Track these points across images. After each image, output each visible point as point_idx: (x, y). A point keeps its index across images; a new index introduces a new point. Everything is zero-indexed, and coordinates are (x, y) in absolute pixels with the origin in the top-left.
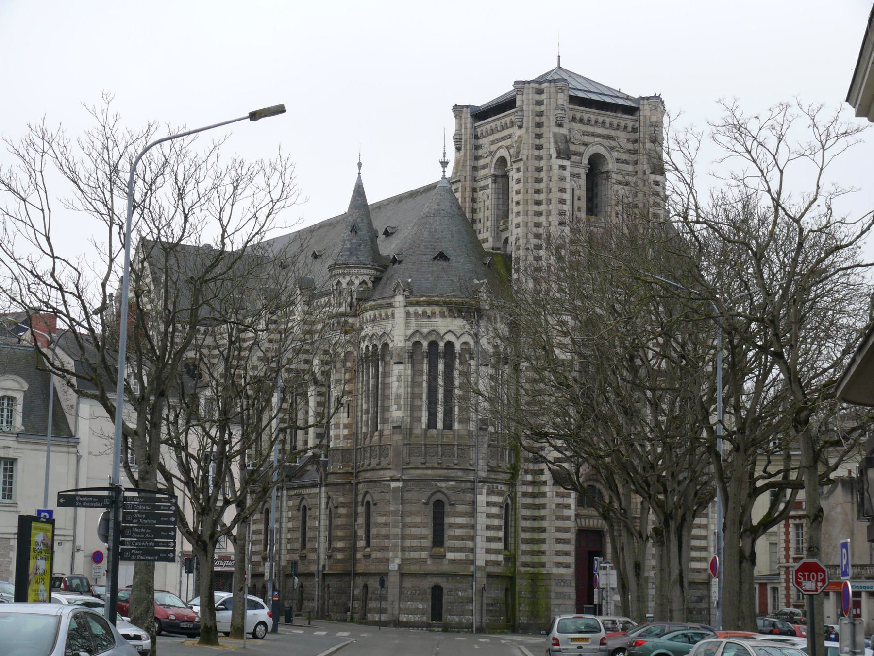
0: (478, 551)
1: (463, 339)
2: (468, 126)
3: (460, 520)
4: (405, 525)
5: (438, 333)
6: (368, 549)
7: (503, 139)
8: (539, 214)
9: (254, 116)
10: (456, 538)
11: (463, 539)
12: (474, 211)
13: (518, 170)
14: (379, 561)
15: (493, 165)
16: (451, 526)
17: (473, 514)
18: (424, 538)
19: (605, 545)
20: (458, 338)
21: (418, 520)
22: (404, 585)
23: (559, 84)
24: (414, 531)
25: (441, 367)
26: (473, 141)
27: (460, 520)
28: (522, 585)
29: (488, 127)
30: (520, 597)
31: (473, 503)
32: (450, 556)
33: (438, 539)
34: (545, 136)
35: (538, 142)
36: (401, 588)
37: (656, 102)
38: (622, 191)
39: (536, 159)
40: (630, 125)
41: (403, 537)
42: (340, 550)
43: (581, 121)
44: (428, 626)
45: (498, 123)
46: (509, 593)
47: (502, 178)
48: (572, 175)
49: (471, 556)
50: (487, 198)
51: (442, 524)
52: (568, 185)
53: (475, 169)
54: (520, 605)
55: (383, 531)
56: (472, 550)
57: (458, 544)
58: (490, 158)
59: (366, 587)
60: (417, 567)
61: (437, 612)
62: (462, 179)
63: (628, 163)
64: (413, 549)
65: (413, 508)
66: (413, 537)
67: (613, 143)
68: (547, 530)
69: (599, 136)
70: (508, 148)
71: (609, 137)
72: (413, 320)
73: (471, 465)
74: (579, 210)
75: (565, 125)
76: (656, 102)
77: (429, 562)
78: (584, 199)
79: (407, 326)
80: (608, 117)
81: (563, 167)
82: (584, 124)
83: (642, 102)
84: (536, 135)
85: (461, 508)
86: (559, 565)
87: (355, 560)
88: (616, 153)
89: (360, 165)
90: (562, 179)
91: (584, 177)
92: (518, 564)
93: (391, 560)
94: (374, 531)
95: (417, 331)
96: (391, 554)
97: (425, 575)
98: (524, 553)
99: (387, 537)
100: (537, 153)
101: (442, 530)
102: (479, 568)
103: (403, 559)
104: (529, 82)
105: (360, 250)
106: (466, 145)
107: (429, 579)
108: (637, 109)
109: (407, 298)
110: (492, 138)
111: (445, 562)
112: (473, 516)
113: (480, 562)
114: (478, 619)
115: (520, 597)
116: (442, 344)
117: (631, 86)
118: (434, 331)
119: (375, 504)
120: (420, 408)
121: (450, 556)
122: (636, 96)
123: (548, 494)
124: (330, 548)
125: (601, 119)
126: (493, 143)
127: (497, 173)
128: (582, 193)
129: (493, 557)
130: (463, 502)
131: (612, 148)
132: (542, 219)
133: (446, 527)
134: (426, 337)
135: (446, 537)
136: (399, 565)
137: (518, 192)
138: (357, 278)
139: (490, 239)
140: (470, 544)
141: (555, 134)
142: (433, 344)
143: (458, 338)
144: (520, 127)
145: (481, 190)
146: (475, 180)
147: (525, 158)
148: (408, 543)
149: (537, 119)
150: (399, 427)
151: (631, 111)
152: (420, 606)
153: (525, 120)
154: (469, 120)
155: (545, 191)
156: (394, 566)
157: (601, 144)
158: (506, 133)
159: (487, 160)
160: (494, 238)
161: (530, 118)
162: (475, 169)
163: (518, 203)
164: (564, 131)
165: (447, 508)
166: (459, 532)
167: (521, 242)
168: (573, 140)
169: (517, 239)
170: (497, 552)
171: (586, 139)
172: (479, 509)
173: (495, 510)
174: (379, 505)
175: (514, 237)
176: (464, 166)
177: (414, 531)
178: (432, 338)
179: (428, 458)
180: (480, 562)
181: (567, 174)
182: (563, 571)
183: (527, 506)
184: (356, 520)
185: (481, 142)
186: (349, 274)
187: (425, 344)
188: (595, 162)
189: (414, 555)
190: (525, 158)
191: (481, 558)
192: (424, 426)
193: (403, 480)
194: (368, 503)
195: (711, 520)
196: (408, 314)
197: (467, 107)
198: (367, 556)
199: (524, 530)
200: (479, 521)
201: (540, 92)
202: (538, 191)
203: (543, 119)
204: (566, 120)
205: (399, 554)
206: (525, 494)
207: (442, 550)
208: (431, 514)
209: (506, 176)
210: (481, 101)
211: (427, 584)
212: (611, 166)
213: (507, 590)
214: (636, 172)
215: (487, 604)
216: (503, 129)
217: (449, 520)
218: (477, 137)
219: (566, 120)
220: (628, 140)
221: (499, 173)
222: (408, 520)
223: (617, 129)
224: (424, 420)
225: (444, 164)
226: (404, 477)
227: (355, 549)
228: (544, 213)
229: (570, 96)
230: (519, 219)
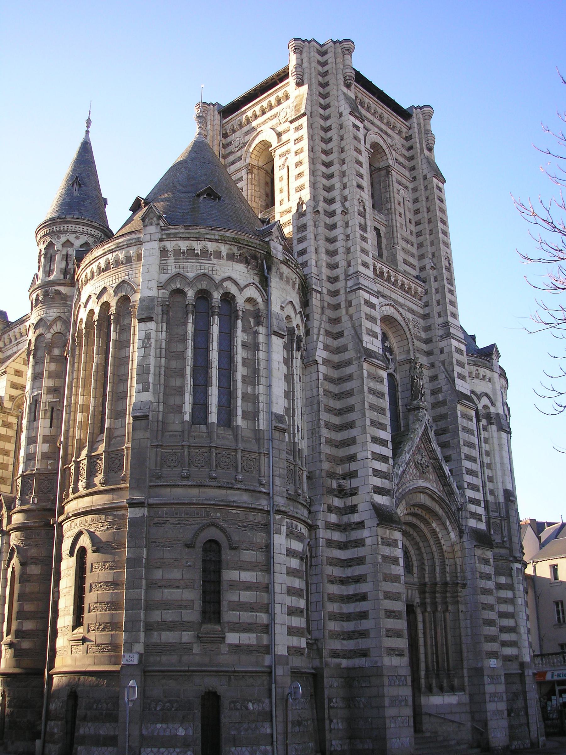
3: (247, 576)
4: (152, 585)
5: (211, 279)
11: (252, 610)
17: (267, 566)
18: (186, 607)
20: (241, 290)
21: (176, 574)
24: (169, 594)
25: (215, 330)
27: (247, 576)
30: (330, 708)
32: (232, 638)
49: (265, 640)
51: (218, 582)
56: (268, 629)
57: (246, 617)
60: (174, 658)
63: (405, 168)
64: (166, 626)
66: (166, 605)
68: (370, 596)
72: (171, 260)
73: (261, 484)
77: (196, 649)
79: (162, 268)
85: (248, 555)
89: (89, 122)
92: (325, 653)
95: (178, 275)
97: (189, 674)
98: (334, 635)
102: (280, 660)
103: (147, 646)
105: (84, 205)
109: (162, 230)
111: (224, 649)
113: (281, 650)
115: (330, 708)
116: (216, 296)
118: (205, 275)
120: (181, 392)
121: (232, 638)
123: (368, 541)
133: (224, 586)
134: (191, 283)
138: (77, 238)
140: (263, 618)
142: (203, 296)
143: (241, 290)
148: (156, 616)
150: (146, 417)
152: (181, 732)
154: (218, 117)
165: (227, 555)
166: (246, 596)
173: (295, 563)
177: (169, 594)
178: (204, 285)
179: (193, 469)
180: (281, 650)
183: (333, 562)
185: (229, 139)
186: (66, 232)
187: (191, 294)
189: (168, 637)
191: (283, 643)
192: (187, 418)
193: (150, 505)
195: (517, 593)
196: (164, 252)
199: (332, 598)
205: (142, 635)
206: (330, 543)
207: (218, 627)
208: (199, 565)
215: (293, 722)
217: (230, 575)
222: (158, 574)
224: (188, 408)
226: (151, 501)
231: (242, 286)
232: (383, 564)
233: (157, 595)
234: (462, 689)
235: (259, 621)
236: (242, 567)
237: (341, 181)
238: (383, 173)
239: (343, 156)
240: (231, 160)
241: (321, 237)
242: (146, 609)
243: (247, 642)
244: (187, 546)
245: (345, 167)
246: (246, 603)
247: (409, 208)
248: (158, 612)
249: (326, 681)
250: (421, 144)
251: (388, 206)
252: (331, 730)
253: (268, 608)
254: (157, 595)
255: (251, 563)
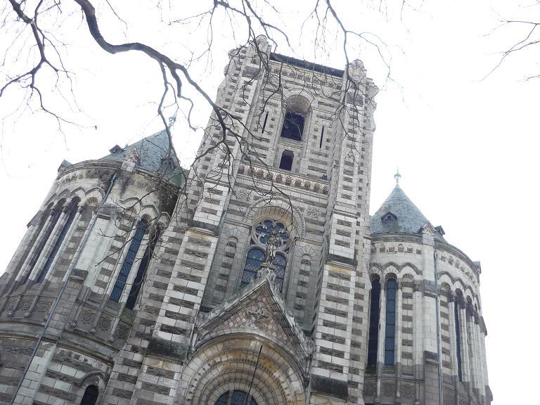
1: (91, 195)
17: (17, 382)
31: (24, 369)
63: (333, 107)
73: (45, 320)
231: (87, 191)
232: (143, 390)
255: (8, 378)
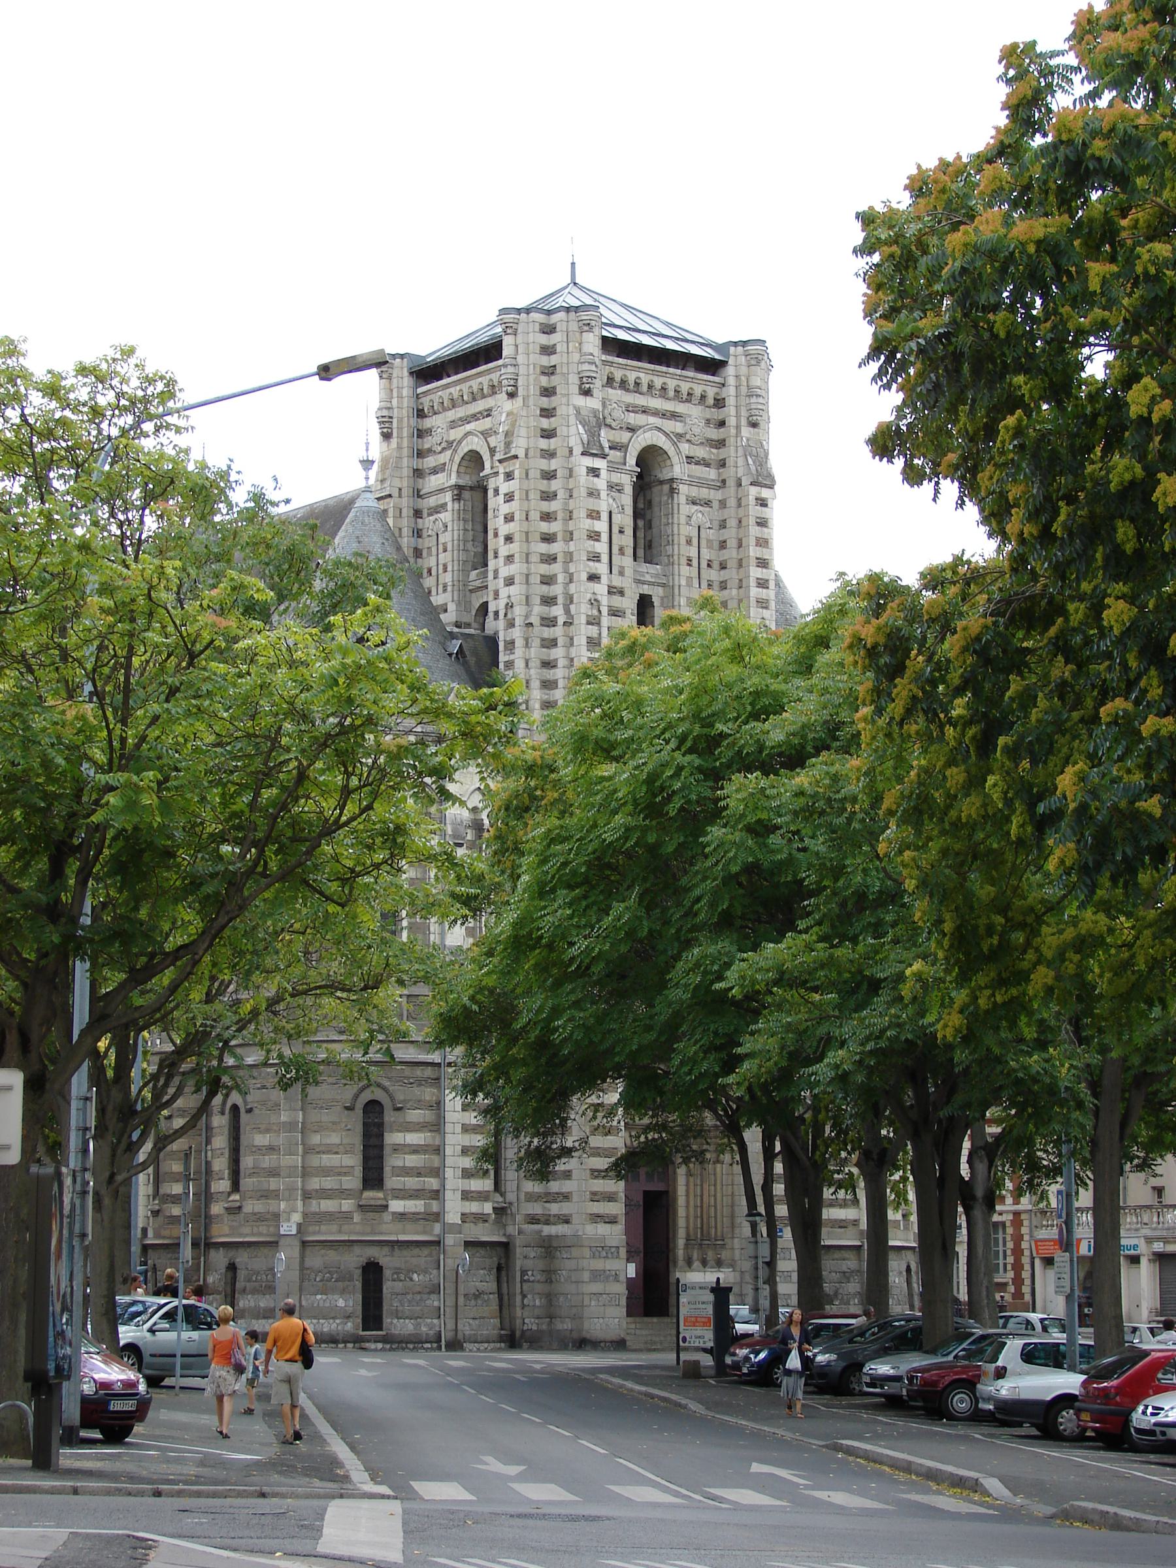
0: (449, 1195)
2: (405, 392)
3: (413, 1138)
4: (308, 1150)
6: (236, 1197)
7: (475, 417)
8: (550, 559)
9: (326, 372)
10: (406, 1171)
11: (419, 1175)
12: (418, 553)
13: (509, 476)
14: (259, 1218)
15: (455, 468)
16: (397, 1148)
17: (437, 1126)
18: (345, 1174)
19: (675, 1180)
21: (334, 1139)
22: (309, 1262)
23: (584, 316)
24: (328, 1160)
26: (413, 422)
27: (413, 1138)
28: (525, 1258)
29: (445, 394)
32: (396, 1206)
33: (373, 1176)
34: (558, 412)
35: (545, 423)
36: (302, 1268)
37: (754, 352)
38: (700, 516)
39: (543, 457)
40: (711, 392)
41: (306, 1173)
42: (176, 1199)
43: (623, 384)
44: (357, 1342)
45: (465, 387)
46: (504, 1273)
47: (474, 493)
48: (611, 487)
49: (435, 1206)
50: (446, 524)
52: (604, 504)
53: (418, 473)
54: (524, 1296)
55: (267, 1161)
56: (437, 1195)
57: (412, 1182)
58: (449, 453)
59: (232, 1268)
61: (372, 1315)
62: (395, 494)
63: (708, 465)
64: (325, 1194)
65: (326, 1117)
66: (326, 1172)
67: (678, 427)
69: (656, 413)
70: (486, 434)
71: (674, 416)
74: (621, 551)
75: (595, 392)
76: (754, 352)
77: (357, 1218)
78: (629, 531)
80: (671, 378)
81: (594, 472)
82: (628, 390)
83: (732, 349)
84: (542, 410)
85: (415, 1115)
86: (596, 1218)
87: (208, 1217)
88: (687, 445)
90: (593, 493)
91: (629, 490)
93: (283, 1217)
94: (247, 1162)
96: (283, 1205)
99: (274, 1173)
100: (543, 444)
101: (381, 1157)
104: (527, 311)
106: (400, 429)
107: (357, 1250)
108: (722, 364)
110: (452, 415)
111: (387, 1217)
112: (438, 1131)
113: (453, 1217)
114: (451, 1325)
117: (706, 323)
119: (250, 1111)
121: (396, 1206)
122: (720, 340)
124: (156, 1193)
125: (658, 382)
126: (453, 425)
127: (461, 482)
128: (625, 519)
129: (474, 1207)
130: (419, 1104)
131: (680, 436)
132: (556, 568)
133: (387, 1151)
135: (387, 1170)
136: (299, 1225)
137: (509, 518)
139: (452, 607)
141: (578, 411)
144: (512, 395)
145: (430, 515)
146: (418, 494)
147: (521, 454)
148: (315, 1183)
149: (544, 381)
151: (711, 366)
152: (341, 1303)
153: (520, 383)
154: (407, 381)
155: (560, 516)
156: (289, 1228)
157: (660, 429)
158: (480, 405)
159: (444, 457)
160: (459, 604)
161: (532, 378)
162: (418, 473)
163: (509, 539)
164: (593, 403)
165: (389, 1116)
166: (412, 1160)
167: (518, 612)
168: (608, 421)
169: (509, 606)
170: (482, 1196)
171: (633, 419)
172: (449, 1117)
174: (256, 1111)
175: (502, 603)
176: (398, 468)
177: (328, 1160)
180: (453, 1217)
181: (601, 484)
182: (603, 1229)
184: (208, 1142)
185: (428, 423)
188: (649, 459)
189: (328, 1205)
190: (521, 454)
194: (235, 1108)
197: (402, 356)
198: (235, 1210)
200: (449, 1139)
201: (549, 330)
202: (547, 517)
203: (555, 380)
204: (598, 383)
205: (300, 1203)
207: (380, 1195)
208: (359, 1128)
209: (481, 489)
210: (431, 343)
211: (354, 1260)
212: (678, 469)
213: (499, 1269)
214: (724, 481)
216: (474, 399)
217: (393, 1138)
218: (421, 414)
219: (598, 383)
220: (708, 421)
221: (465, 481)
222: (316, 1139)
223: (687, 401)
225: (367, 464)
227: (206, 1196)
228: (560, 558)
229: (604, 338)
230: (514, 569)
233: (315, 1161)
234: (732, 1265)
235: (427, 1187)
236: (408, 1128)
237: (566, 571)
238: (666, 487)
239: (571, 526)
240: (432, 465)
241: (535, 663)
242: (304, 1176)
243: (413, 1210)
244: (347, 1108)
245: (572, 546)
246: (412, 1168)
247: (708, 541)
248: (316, 1180)
249: (518, 1250)
250: (738, 416)
251: (669, 548)
252: (523, 1306)
253: (438, 1172)
254: (315, 1161)
